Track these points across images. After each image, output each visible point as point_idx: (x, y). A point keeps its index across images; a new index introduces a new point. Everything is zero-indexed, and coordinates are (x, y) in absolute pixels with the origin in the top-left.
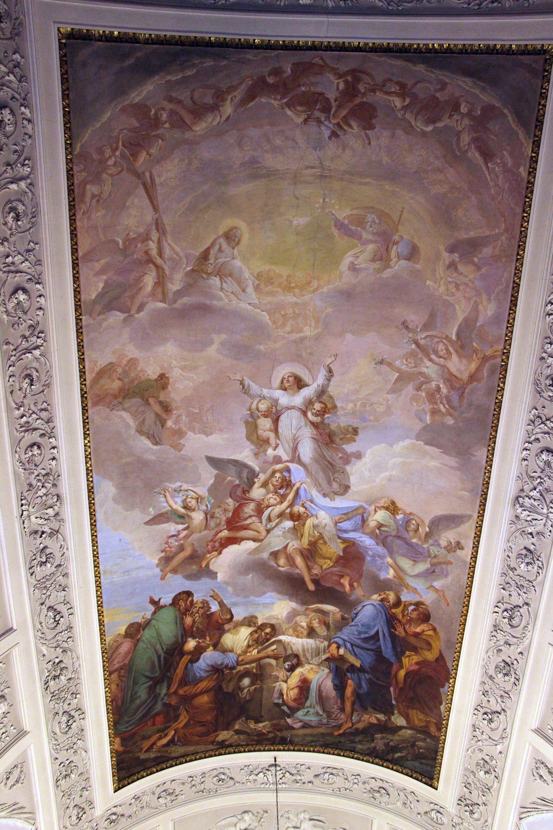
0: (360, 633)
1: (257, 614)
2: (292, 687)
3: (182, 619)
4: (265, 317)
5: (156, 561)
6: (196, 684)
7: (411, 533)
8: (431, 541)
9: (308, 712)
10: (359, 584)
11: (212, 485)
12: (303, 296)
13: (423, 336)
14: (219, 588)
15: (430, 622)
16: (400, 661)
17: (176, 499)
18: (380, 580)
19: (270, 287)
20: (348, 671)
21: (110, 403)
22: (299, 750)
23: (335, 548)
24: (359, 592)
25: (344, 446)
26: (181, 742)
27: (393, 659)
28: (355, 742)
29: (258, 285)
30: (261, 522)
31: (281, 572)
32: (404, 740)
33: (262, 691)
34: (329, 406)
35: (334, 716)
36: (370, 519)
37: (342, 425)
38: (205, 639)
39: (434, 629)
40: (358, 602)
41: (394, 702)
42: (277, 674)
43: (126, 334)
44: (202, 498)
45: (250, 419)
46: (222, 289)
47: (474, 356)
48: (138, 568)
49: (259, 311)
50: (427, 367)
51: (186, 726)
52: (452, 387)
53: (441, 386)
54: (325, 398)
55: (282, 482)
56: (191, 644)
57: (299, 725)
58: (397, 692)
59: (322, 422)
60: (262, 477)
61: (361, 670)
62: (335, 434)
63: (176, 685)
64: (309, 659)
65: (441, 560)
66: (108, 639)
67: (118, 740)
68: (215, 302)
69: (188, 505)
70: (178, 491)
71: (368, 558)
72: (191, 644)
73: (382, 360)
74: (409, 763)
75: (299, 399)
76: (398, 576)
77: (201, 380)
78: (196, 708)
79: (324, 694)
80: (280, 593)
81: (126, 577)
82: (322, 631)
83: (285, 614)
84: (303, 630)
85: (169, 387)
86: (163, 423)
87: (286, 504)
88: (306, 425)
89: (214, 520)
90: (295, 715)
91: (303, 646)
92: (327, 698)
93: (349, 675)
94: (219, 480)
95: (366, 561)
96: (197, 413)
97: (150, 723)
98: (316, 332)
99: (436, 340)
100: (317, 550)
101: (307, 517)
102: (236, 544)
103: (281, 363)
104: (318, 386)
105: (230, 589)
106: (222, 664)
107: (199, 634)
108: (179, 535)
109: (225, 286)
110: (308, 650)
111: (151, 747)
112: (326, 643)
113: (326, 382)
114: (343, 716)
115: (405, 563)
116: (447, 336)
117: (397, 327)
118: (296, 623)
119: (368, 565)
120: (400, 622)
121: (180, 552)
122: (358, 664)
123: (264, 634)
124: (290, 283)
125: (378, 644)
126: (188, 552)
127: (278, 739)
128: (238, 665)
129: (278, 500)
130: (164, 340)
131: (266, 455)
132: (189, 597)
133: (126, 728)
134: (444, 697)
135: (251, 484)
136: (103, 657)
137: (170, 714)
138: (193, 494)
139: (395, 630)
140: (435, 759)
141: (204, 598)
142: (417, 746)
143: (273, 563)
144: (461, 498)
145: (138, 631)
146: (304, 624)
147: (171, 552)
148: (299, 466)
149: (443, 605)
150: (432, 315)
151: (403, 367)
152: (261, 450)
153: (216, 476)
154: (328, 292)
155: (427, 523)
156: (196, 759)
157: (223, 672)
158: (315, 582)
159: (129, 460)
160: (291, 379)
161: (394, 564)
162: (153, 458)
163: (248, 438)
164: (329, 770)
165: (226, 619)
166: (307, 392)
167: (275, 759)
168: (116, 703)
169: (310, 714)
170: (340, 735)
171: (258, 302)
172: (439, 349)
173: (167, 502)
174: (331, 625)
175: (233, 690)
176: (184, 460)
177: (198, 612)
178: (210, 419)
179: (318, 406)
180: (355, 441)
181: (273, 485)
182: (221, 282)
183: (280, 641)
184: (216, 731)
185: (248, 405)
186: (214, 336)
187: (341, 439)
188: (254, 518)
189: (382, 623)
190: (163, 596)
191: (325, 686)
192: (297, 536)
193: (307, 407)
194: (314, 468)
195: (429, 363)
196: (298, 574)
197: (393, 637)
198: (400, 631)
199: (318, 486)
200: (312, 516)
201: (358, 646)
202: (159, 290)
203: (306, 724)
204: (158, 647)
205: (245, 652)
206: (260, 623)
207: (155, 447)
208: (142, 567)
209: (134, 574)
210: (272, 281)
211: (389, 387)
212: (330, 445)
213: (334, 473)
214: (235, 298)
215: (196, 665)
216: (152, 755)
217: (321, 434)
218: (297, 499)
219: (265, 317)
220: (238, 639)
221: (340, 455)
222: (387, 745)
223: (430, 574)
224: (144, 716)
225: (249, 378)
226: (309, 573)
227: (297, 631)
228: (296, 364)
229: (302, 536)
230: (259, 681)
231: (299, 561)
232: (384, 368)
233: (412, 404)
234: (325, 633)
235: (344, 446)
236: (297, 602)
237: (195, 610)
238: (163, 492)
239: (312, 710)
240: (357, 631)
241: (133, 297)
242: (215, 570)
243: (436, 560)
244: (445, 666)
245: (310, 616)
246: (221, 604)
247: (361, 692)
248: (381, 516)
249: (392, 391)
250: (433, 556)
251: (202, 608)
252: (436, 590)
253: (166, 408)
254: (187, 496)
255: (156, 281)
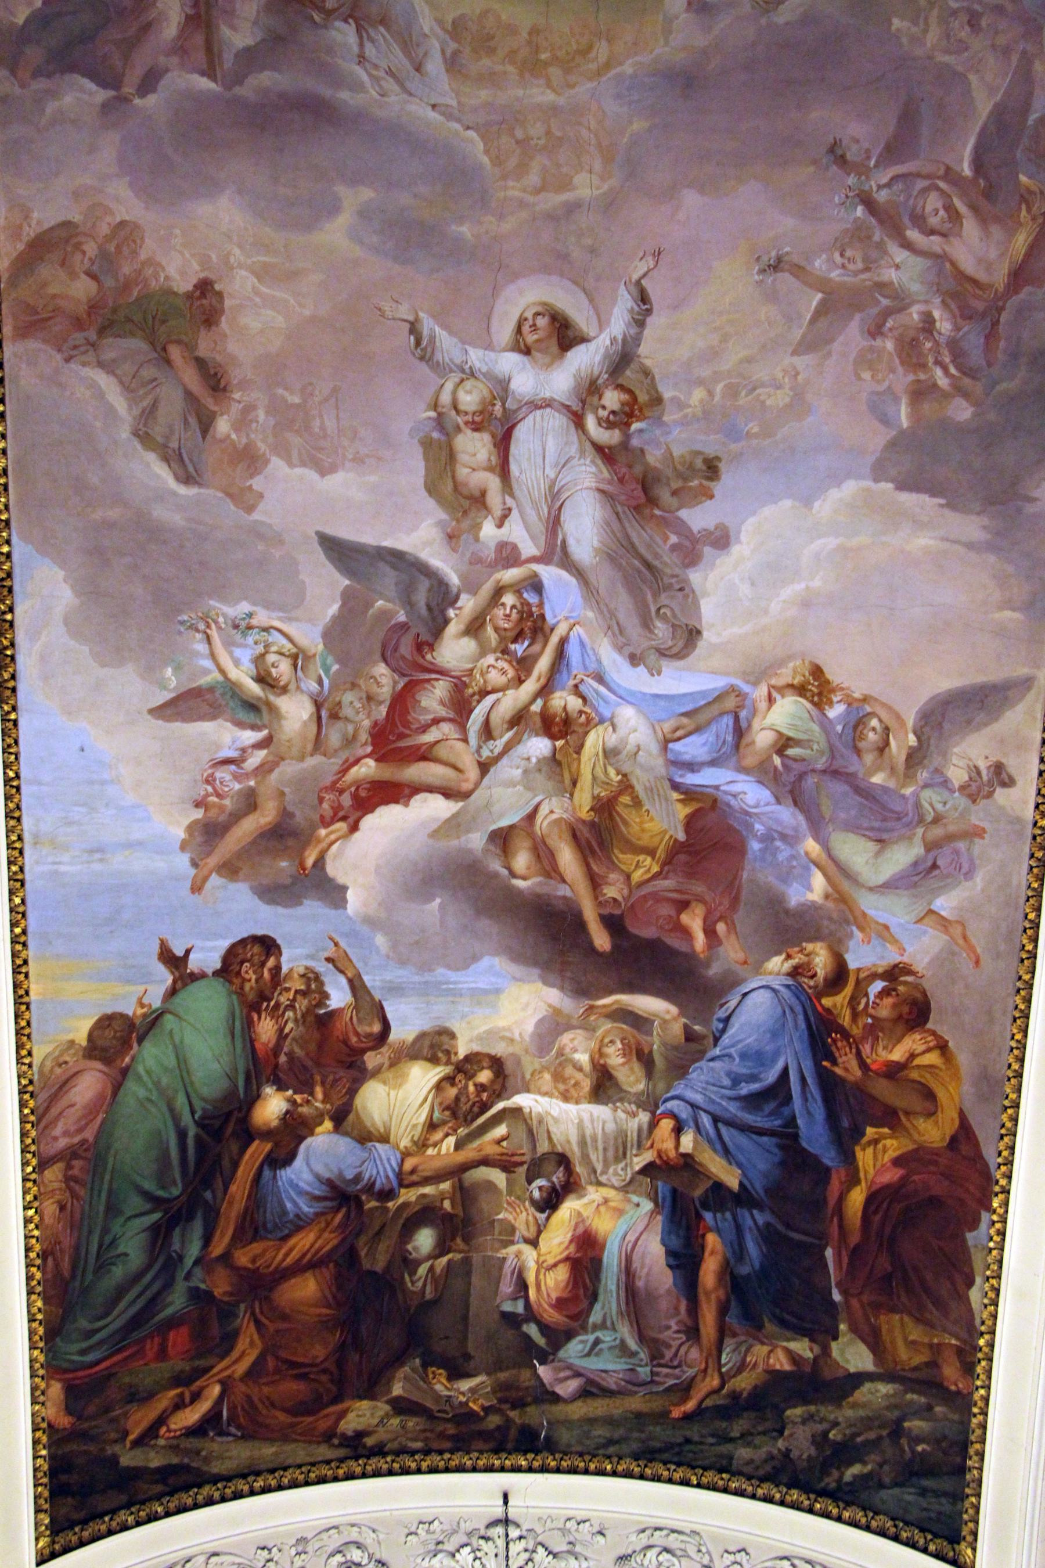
0: (736, 1080)
1: (456, 1026)
2: (551, 1261)
3: (249, 1025)
4: (474, 145)
5: (181, 834)
6: (285, 1238)
7: (869, 758)
8: (923, 775)
9: (597, 1342)
10: (732, 927)
11: (336, 620)
12: (571, 86)
13: (884, 180)
14: (352, 934)
15: (930, 1025)
16: (849, 1158)
17: (238, 652)
18: (787, 912)
19: (486, 62)
20: (705, 1206)
21: (65, 341)
22: (573, 1471)
23: (663, 820)
24: (732, 951)
25: (684, 514)
26: (239, 1427)
27: (829, 1157)
28: (732, 1440)
29: (456, 54)
30: (465, 740)
31: (519, 892)
32: (869, 1418)
33: (468, 1274)
34: (642, 397)
35: (668, 1354)
36: (756, 724)
37: (676, 453)
38: (312, 1093)
39: (943, 1047)
40: (730, 982)
41: (837, 1296)
42: (510, 1217)
43: (109, 147)
44: (308, 658)
45: (435, 435)
46: (362, 59)
47: (1024, 212)
48: (130, 845)
49: (456, 126)
50: (897, 267)
51: (253, 1373)
52: (965, 314)
53: (936, 314)
54: (630, 375)
55: (521, 619)
56: (273, 1106)
57: (573, 1385)
58: (845, 1260)
59: (625, 445)
60: (468, 604)
61: (743, 1198)
62: (657, 480)
63: (227, 1240)
64: (599, 1168)
65: (952, 828)
66: (40, 1051)
67: (56, 1389)
68: (344, 95)
69: (269, 674)
70: (242, 627)
71: (755, 846)
72: (273, 1106)
73: (779, 260)
74: (884, 1494)
75: (561, 379)
76: (838, 896)
77: (307, 313)
78: (285, 1317)
79: (640, 1284)
80: (517, 957)
81: (97, 867)
82: (631, 1078)
83: (529, 1027)
84: (579, 1076)
85: (224, 323)
86: (206, 425)
87: (530, 686)
88: (582, 453)
89: (340, 725)
90: (561, 1354)
91: (580, 1126)
92: (651, 1296)
93: (708, 1216)
94: (353, 606)
95: (750, 855)
96: (298, 406)
97: (151, 1348)
98: (606, 187)
99: (921, 184)
100: (615, 826)
101: (589, 724)
102: (397, 802)
103: (515, 276)
104: (613, 341)
105: (380, 940)
106: (358, 1178)
107: (295, 1077)
108: (244, 760)
109: (370, 50)
110: (595, 1139)
111: (152, 1432)
112: (644, 1117)
113: (633, 331)
114: (694, 1354)
115: (855, 851)
116: (948, 169)
117: (815, 162)
118: (560, 1053)
119: (757, 870)
120: (846, 1035)
121: (246, 814)
122: (732, 1179)
123: (477, 1086)
124: (537, 50)
125: (786, 1111)
126: (265, 816)
127: (513, 1433)
128: (401, 1185)
129: (511, 673)
130: (211, 187)
131: (477, 539)
132: (268, 955)
133: (83, 1352)
134: (977, 1264)
135: (438, 625)
136: (22, 1105)
137: (210, 1328)
138: (284, 641)
139: (835, 1063)
140: (962, 1470)
141: (311, 963)
142: (908, 1434)
143: (496, 865)
144: (1000, 631)
145: (125, 1044)
146: (583, 1058)
147: (222, 808)
148: (564, 574)
149: (965, 965)
150: (908, 118)
151: (835, 275)
152: (465, 524)
153: (347, 596)
154: (634, 76)
155: (910, 723)
156: (280, 1488)
157: (360, 1204)
158: (613, 924)
159: (113, 514)
160: (542, 322)
161: (824, 856)
162: (177, 519)
163: (432, 489)
164: (658, 1538)
165: (369, 1035)
166: (585, 359)
167: (506, 1497)
168: (57, 1265)
169: (602, 1352)
170: (687, 1417)
171: (454, 103)
172: (928, 209)
173: (213, 656)
174: (657, 1057)
175: (388, 1269)
176: (260, 536)
177: (291, 1007)
178: (330, 424)
179: (612, 399)
180: (712, 497)
181: (496, 629)
182: (361, 37)
183: (518, 1111)
184: (337, 1399)
185: (429, 394)
186: (341, 190)
187: (675, 493)
188: (446, 728)
189: (797, 1045)
190: (198, 943)
191: (643, 1257)
192: (562, 782)
193: (583, 402)
194: (604, 578)
195: (900, 255)
196: (565, 898)
197: (830, 1087)
198: (847, 1067)
199: (616, 631)
200: (601, 721)
201: (730, 1123)
202: (199, 39)
203: (590, 1382)
204: (181, 1101)
205: (422, 1145)
206: (462, 1053)
207: (182, 490)
208: (140, 844)
209: (118, 861)
210: (492, 44)
211: (797, 334)
212: (647, 511)
213: (656, 595)
214: (396, 88)
215: (286, 1174)
216: (156, 1461)
217: (621, 480)
218: (559, 671)
219: (474, 145)
220: (401, 1100)
221: (674, 539)
222: (820, 1440)
223: (925, 874)
224: (135, 1322)
225: (433, 317)
226: (596, 898)
227: (564, 1080)
228: (555, 279)
229: (574, 783)
230: (459, 1240)
231: (567, 858)
232: (785, 280)
233: (859, 378)
234: (641, 1086)
235: (684, 514)
236: (562, 989)
237: (284, 999)
238: (202, 626)
239: (607, 1337)
240: (729, 1074)
241: (130, 46)
242: (341, 880)
243: (937, 832)
244: (977, 1159)
245: (599, 1033)
246: (356, 985)
247: (744, 1270)
248: (785, 714)
249: (803, 347)
250: (929, 818)
251: (304, 993)
252: (944, 924)
253: (216, 380)
254: (267, 646)
255: (190, 11)
